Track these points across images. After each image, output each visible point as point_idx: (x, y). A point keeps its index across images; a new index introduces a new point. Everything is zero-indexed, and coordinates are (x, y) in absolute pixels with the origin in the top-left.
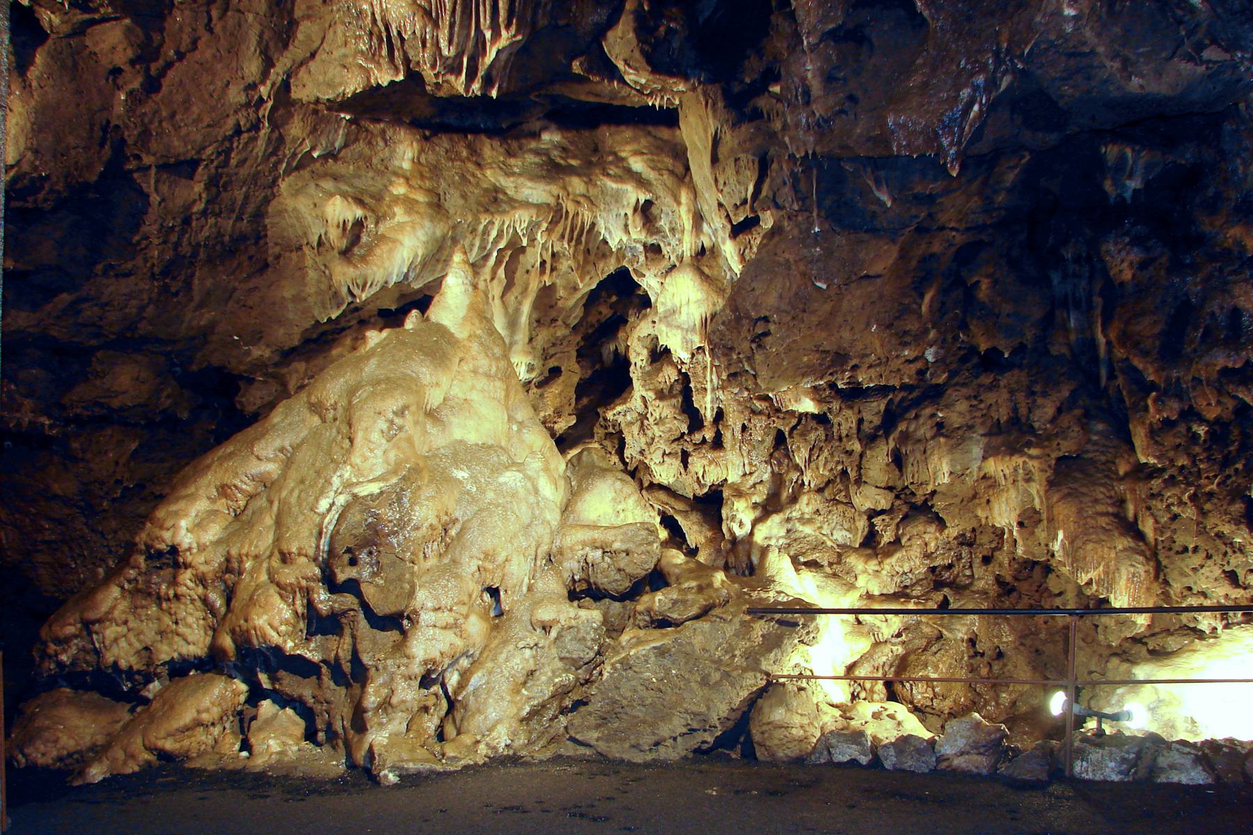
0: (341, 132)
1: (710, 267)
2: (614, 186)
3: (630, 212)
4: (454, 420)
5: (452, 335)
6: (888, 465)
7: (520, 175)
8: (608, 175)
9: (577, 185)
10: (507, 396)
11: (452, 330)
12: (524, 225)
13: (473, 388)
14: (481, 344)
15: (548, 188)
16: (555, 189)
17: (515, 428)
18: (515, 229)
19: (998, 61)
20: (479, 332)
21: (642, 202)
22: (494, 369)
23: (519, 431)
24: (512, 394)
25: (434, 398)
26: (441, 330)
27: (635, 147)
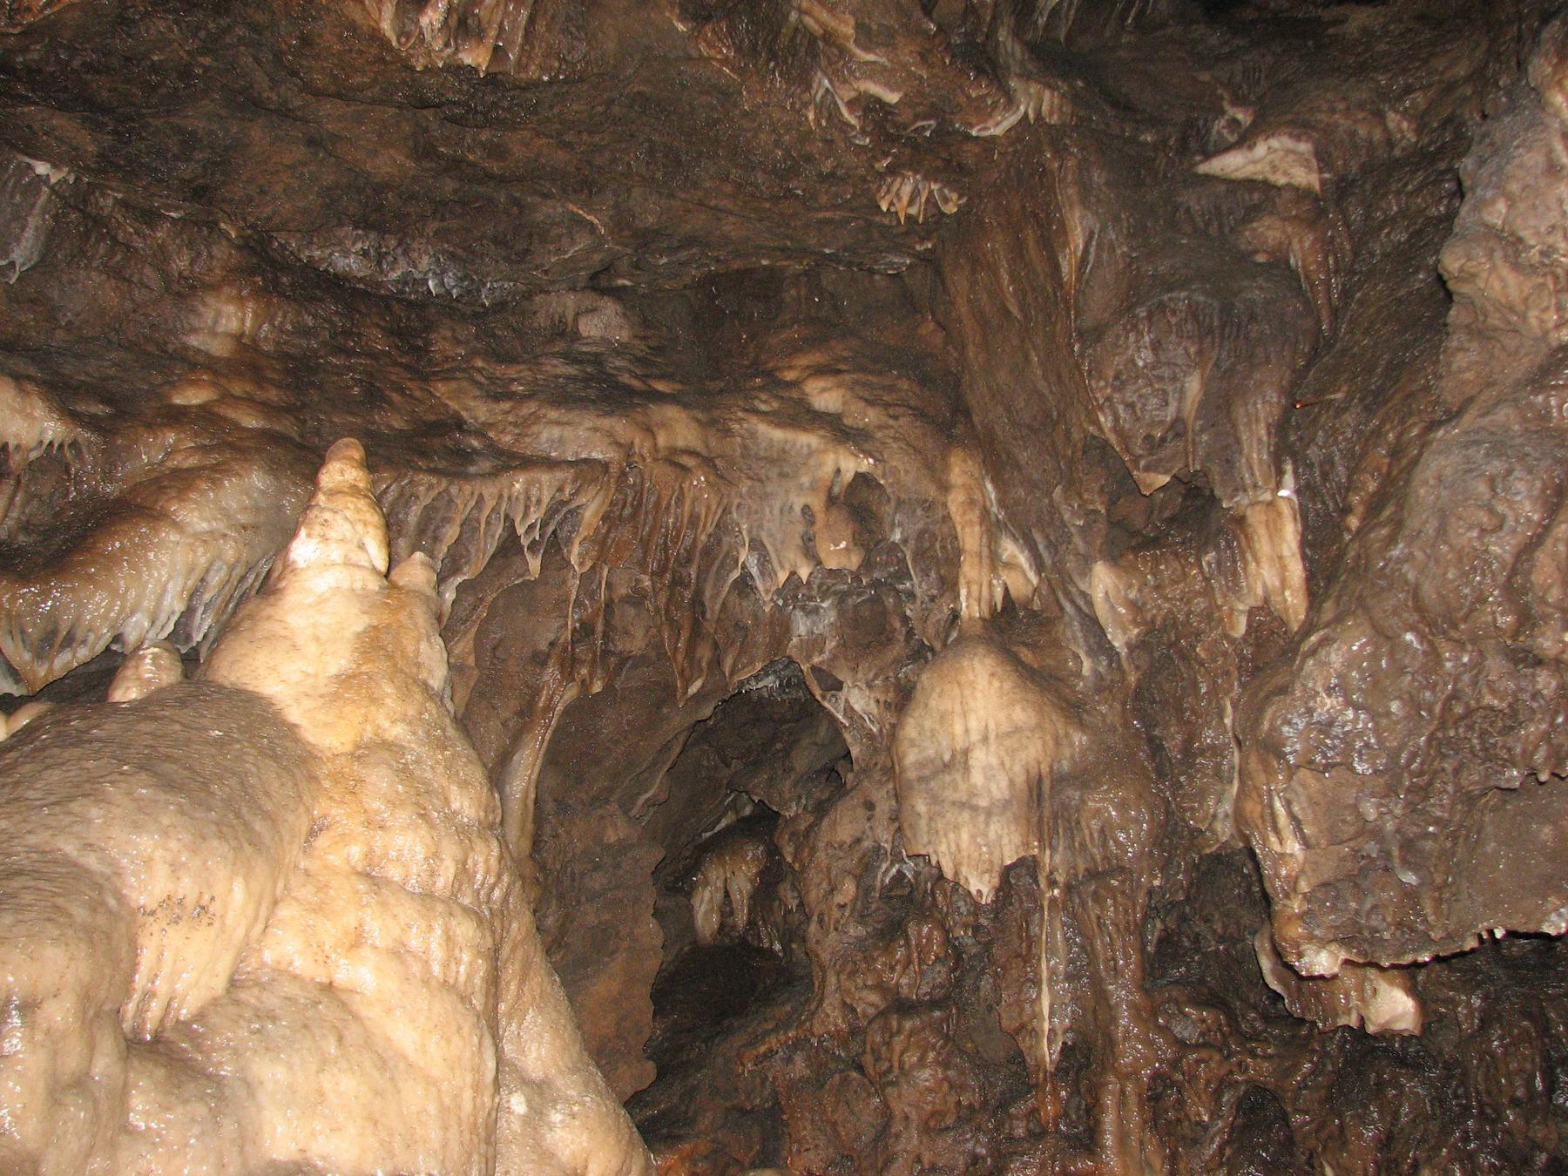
0: (33, 221)
1: (1033, 647)
2: (778, 434)
3: (817, 503)
4: (271, 1073)
5: (290, 731)
6: (291, 964)
7: (529, 397)
8: (756, 412)
9: (679, 428)
10: (494, 981)
11: (294, 715)
12: (535, 516)
13: (356, 941)
14: (405, 773)
15: (606, 423)
16: (620, 427)
17: (518, 1104)
18: (509, 522)
19: (558, 881)
20: (397, 732)
21: (848, 476)
22: (447, 871)
23: (536, 1116)
24: (511, 972)
25: (179, 971)
26: (254, 714)
27: (817, 358)
